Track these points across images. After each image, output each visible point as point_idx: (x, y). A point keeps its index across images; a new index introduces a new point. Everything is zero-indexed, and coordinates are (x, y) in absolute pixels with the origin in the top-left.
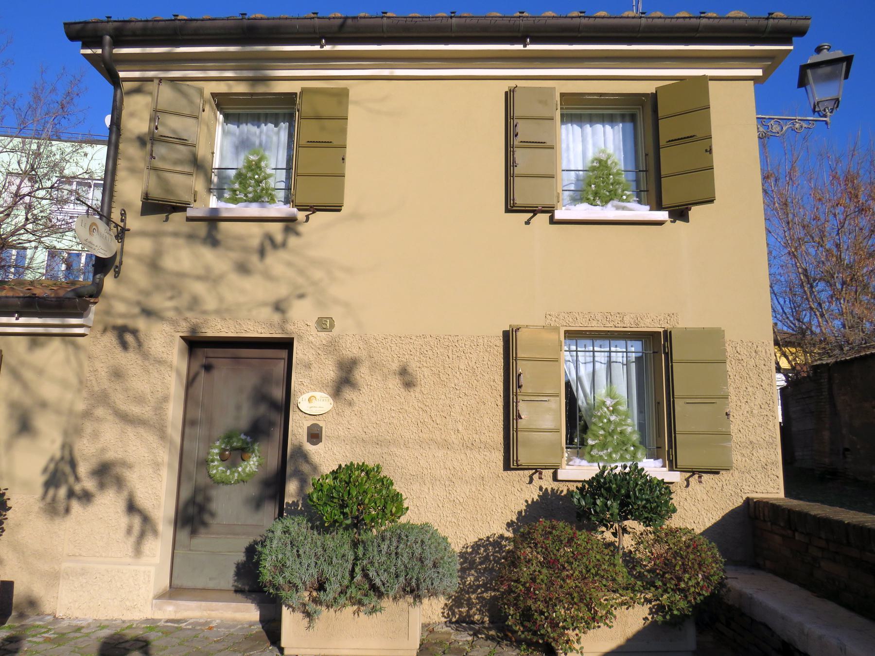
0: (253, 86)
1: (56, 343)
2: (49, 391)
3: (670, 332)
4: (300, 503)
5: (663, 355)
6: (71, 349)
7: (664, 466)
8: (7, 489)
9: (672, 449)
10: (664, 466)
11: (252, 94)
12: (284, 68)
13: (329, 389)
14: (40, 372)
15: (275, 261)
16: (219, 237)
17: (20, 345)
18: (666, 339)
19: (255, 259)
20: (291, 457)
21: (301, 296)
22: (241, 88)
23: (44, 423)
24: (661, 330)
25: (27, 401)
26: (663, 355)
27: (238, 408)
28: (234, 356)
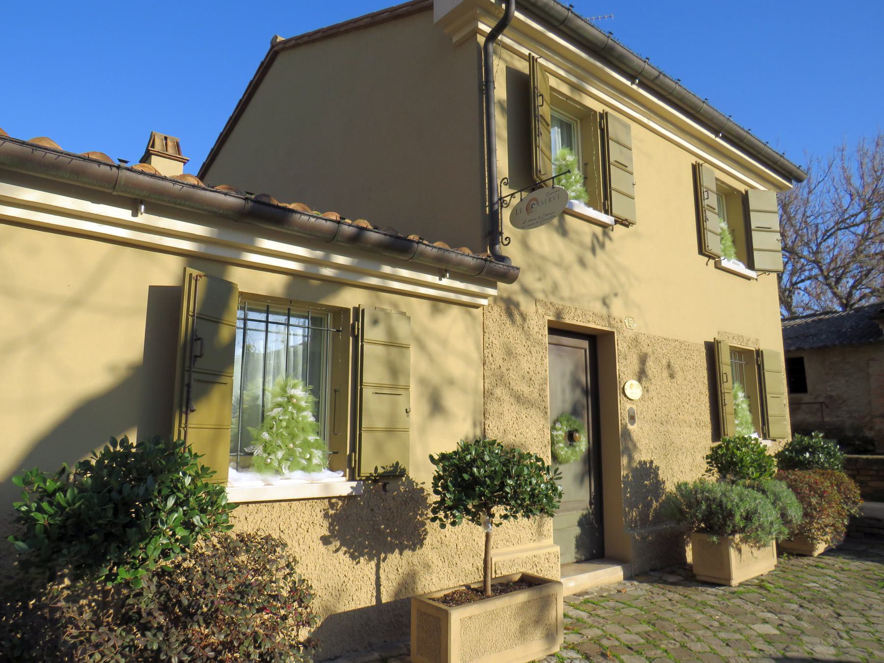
0: (572, 91)
1: (455, 310)
2: (455, 367)
3: (363, 310)
4: (630, 475)
5: (351, 338)
6: (468, 317)
7: (344, 476)
8: (423, 483)
9: (355, 453)
10: (344, 476)
11: (568, 97)
12: (630, 106)
13: (636, 377)
14: (444, 342)
15: (600, 260)
16: (568, 227)
17: (420, 308)
18: (356, 318)
19: (589, 255)
20: (622, 435)
21: (616, 295)
22: (565, 89)
23: (453, 401)
24: (754, 349)
25: (435, 378)
26: (351, 338)
27: (563, 392)
28: (557, 343)
